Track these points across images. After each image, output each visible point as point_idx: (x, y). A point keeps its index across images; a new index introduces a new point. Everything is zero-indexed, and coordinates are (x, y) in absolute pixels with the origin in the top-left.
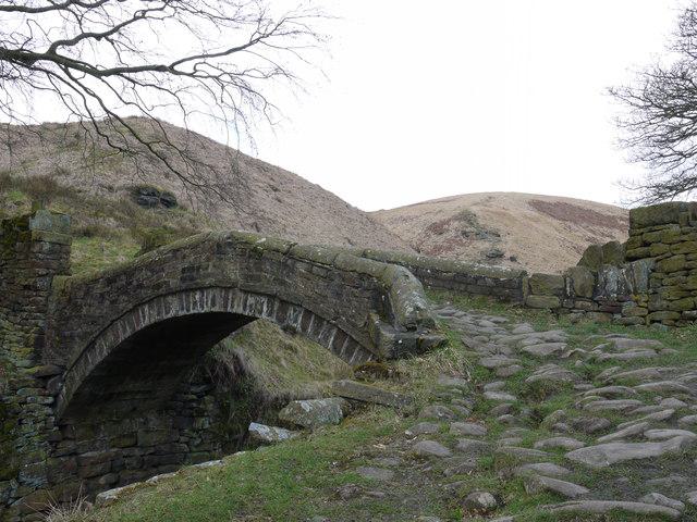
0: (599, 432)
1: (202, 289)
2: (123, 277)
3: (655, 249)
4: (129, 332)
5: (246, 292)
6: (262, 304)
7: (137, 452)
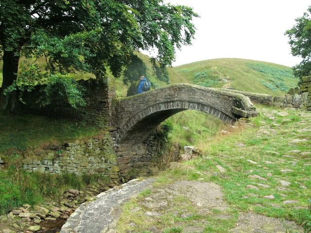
4: (144, 116)
7: (137, 157)
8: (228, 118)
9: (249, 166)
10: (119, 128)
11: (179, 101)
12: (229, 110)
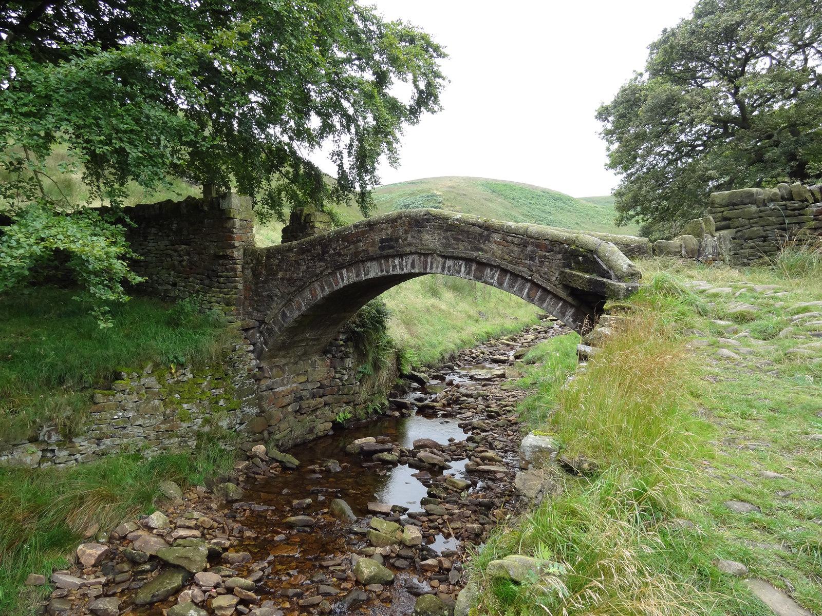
0: (301, 374)
1: (401, 256)
2: (319, 247)
3: (736, 222)
4: (327, 290)
5: (445, 257)
6: (460, 266)
7: (309, 386)
8: (549, 297)
9: (743, 137)
10: (262, 322)
11: (416, 253)
12: (555, 277)
